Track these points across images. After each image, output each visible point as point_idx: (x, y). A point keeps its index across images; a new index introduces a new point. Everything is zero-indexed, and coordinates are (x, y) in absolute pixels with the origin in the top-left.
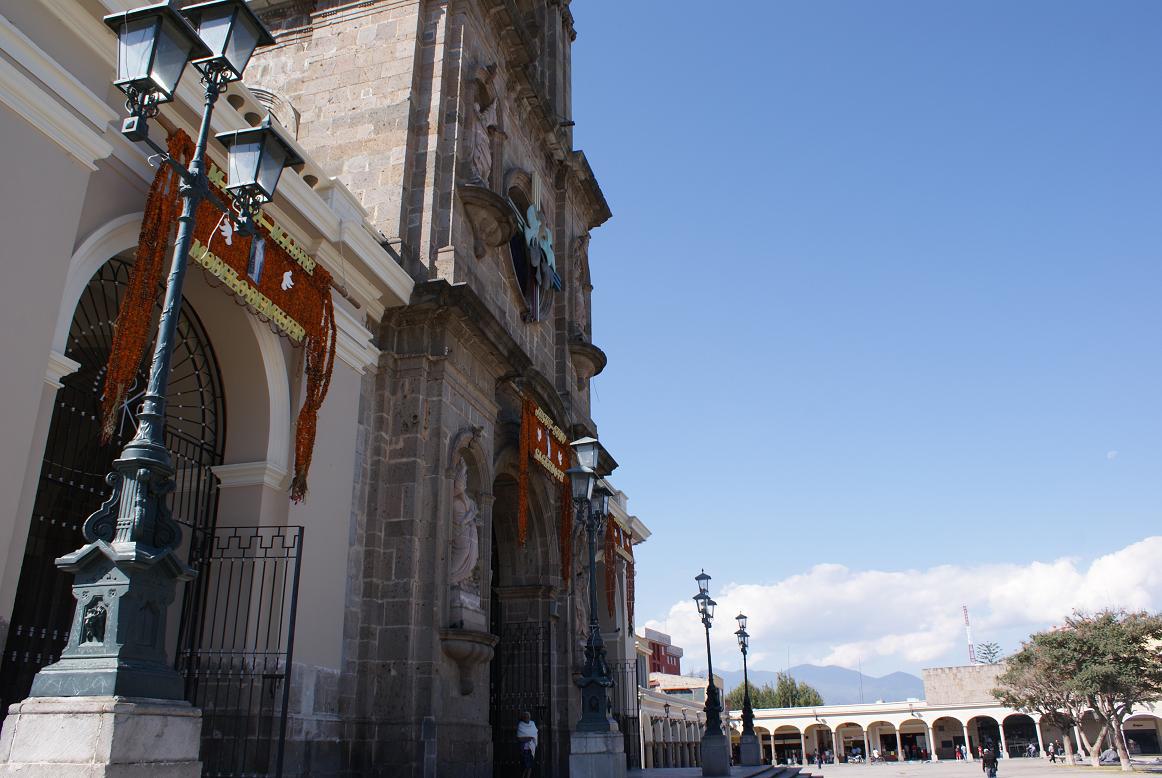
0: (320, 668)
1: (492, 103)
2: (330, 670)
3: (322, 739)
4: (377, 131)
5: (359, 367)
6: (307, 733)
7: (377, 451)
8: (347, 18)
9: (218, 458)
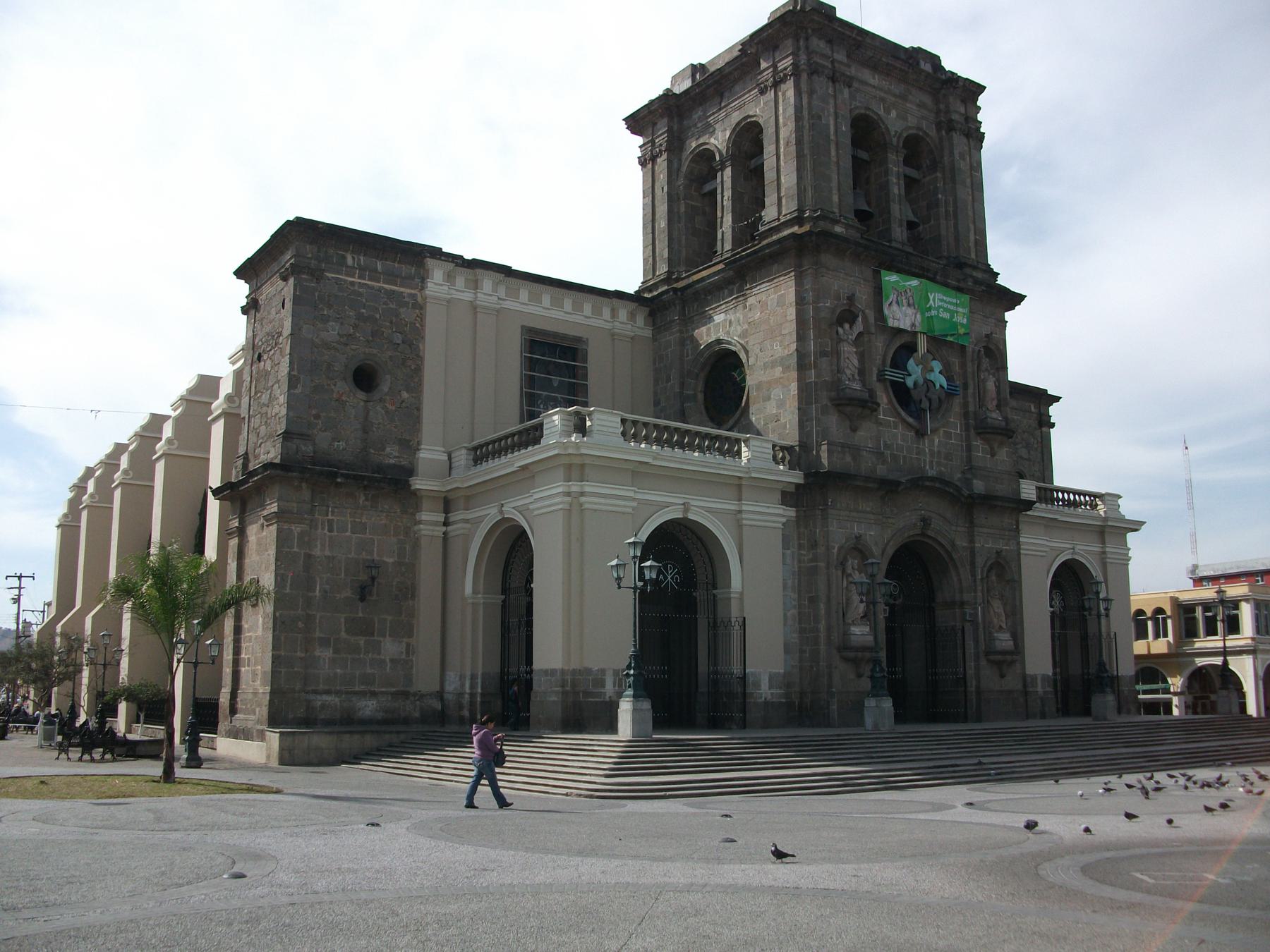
0: (771, 670)
1: (858, 316)
2: (777, 671)
3: (774, 700)
4: (783, 372)
5: (780, 525)
6: (765, 699)
7: (799, 561)
8: (763, 290)
9: (715, 587)
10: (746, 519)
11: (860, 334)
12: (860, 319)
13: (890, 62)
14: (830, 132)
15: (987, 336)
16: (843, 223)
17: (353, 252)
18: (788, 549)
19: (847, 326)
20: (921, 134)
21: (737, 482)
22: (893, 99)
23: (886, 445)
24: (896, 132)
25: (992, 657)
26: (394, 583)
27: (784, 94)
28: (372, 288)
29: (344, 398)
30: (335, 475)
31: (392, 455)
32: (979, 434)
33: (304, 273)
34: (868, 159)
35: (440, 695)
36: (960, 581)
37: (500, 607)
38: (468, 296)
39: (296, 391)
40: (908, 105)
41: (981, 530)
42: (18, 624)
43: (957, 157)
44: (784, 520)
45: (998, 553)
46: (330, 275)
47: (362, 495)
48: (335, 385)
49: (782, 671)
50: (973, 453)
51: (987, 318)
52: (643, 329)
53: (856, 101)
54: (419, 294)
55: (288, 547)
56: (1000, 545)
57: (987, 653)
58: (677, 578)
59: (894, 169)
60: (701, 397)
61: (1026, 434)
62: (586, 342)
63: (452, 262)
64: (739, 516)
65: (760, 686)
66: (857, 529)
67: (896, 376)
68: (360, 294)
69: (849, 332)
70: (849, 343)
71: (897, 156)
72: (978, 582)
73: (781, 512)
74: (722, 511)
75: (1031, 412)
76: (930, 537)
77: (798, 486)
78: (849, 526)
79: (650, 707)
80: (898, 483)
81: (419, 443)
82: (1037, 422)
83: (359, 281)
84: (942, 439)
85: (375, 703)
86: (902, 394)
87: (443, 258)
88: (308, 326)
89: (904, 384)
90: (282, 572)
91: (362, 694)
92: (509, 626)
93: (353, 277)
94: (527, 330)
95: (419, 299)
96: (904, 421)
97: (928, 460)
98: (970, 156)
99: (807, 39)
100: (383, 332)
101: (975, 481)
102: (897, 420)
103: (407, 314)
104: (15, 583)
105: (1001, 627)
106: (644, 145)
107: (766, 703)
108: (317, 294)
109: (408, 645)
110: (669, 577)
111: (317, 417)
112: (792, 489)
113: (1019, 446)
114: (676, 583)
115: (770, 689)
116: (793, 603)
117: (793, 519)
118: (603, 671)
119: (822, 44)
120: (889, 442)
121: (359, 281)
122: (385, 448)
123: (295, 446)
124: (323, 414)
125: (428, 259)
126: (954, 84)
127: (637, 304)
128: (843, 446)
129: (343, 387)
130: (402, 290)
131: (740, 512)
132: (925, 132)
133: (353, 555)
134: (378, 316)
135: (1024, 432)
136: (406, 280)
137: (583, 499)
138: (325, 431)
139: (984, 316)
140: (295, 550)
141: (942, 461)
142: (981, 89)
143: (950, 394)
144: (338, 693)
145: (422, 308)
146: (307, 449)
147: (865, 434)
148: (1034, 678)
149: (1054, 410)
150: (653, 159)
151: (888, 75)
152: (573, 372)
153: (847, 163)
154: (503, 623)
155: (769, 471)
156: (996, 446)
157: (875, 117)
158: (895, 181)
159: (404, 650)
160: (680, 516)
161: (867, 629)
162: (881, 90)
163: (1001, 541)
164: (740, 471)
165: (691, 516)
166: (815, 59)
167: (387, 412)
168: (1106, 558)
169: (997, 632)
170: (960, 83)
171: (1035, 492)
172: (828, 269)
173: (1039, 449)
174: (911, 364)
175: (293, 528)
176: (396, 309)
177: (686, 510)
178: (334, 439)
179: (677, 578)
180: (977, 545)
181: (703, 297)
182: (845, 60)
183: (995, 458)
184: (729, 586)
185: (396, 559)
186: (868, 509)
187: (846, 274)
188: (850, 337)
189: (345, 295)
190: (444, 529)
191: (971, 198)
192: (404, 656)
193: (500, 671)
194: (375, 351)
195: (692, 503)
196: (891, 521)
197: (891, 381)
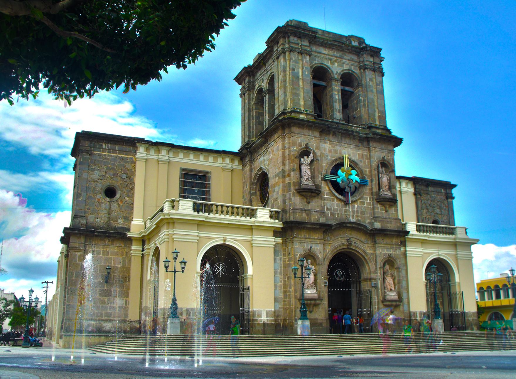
2: (270, 310)
3: (268, 322)
5: (273, 246)
6: (264, 322)
10: (459, 257)
11: (312, 161)
12: (312, 154)
13: (332, 43)
14: (299, 75)
15: (383, 158)
16: (304, 113)
17: (105, 143)
18: (278, 256)
19: (306, 157)
20: (351, 72)
21: (250, 228)
22: (336, 58)
23: (328, 209)
24: (337, 72)
25: (385, 303)
26: (121, 275)
27: (280, 61)
28: (114, 156)
29: (100, 201)
30: (94, 232)
31: (120, 223)
32: (378, 202)
33: (84, 152)
34: (326, 85)
35: (139, 322)
36: (369, 268)
38: (156, 157)
39: (80, 199)
40: (343, 60)
41: (379, 245)
42: (46, 302)
43: (368, 80)
44: (275, 243)
45: (390, 255)
46: (95, 152)
47: (107, 239)
48: (96, 196)
49: (273, 310)
50: (375, 211)
51: (383, 149)
52: (238, 166)
53: (316, 61)
54: (134, 158)
55: (74, 261)
56: (391, 252)
57: (383, 302)
59: (336, 88)
60: (258, 193)
61: (439, 202)
62: (210, 173)
63: (147, 144)
64: (456, 256)
67: (333, 178)
68: (108, 159)
69: (306, 160)
70: (306, 165)
71: (337, 82)
72: (378, 269)
73: (273, 240)
74: (247, 241)
75: (442, 193)
76: (353, 249)
77: (282, 228)
80: (330, 226)
81: (132, 218)
82: (445, 197)
83: (108, 154)
84: (359, 205)
85: (111, 324)
86: (335, 185)
87: (143, 142)
88: (85, 173)
89: (336, 181)
90: (71, 271)
91: (106, 321)
93: (106, 152)
94: (183, 170)
95: (134, 160)
96: (337, 198)
97: (351, 215)
98: (376, 79)
99: (289, 37)
100: (118, 174)
101: (375, 223)
102: (334, 198)
103: (128, 166)
104: (45, 285)
105: (391, 290)
106: (241, 89)
107: (264, 324)
108: (90, 160)
109: (126, 301)
110: (220, 270)
111: (89, 209)
112: (280, 230)
113: (436, 208)
114: (224, 272)
115: (266, 317)
116: (280, 280)
117: (280, 243)
119: (296, 39)
120: (329, 207)
121: (108, 154)
122: (118, 220)
123: (78, 221)
124: (91, 208)
125: (137, 143)
126: (366, 49)
127: (233, 156)
128: (302, 210)
129: (101, 196)
130: (126, 156)
131: (457, 254)
132: (352, 71)
133: (103, 264)
134: (116, 168)
135: (438, 202)
136: (129, 153)
137: (174, 236)
138: (92, 214)
139: (382, 149)
140: (77, 262)
141: (359, 214)
142: (380, 49)
143: (363, 184)
144: (95, 320)
145: (135, 163)
146: (83, 222)
147: (315, 205)
148: (415, 314)
149: (454, 191)
150: (244, 94)
151: (333, 49)
152: (205, 186)
153: (309, 88)
155: (272, 223)
156: (387, 207)
157: (326, 67)
158: (336, 93)
159: (124, 303)
160: (222, 242)
161: (315, 291)
162: (329, 55)
163: (391, 250)
164: (251, 223)
165: (227, 243)
166: (291, 45)
167: (119, 206)
168: (458, 257)
169: (389, 291)
170: (368, 48)
171: (415, 227)
172: (295, 133)
173: (447, 209)
174: (340, 172)
175: (77, 253)
176: (124, 164)
177: (225, 240)
178: (96, 218)
180: (377, 252)
181: (257, 150)
182: (308, 44)
183: (388, 212)
184: (247, 272)
185: (122, 266)
186: (316, 237)
187: (305, 135)
188: (307, 162)
189: (102, 160)
190: (142, 253)
191: (376, 97)
192: (124, 305)
194: (114, 182)
195: (228, 237)
196: (330, 242)
197: (331, 180)
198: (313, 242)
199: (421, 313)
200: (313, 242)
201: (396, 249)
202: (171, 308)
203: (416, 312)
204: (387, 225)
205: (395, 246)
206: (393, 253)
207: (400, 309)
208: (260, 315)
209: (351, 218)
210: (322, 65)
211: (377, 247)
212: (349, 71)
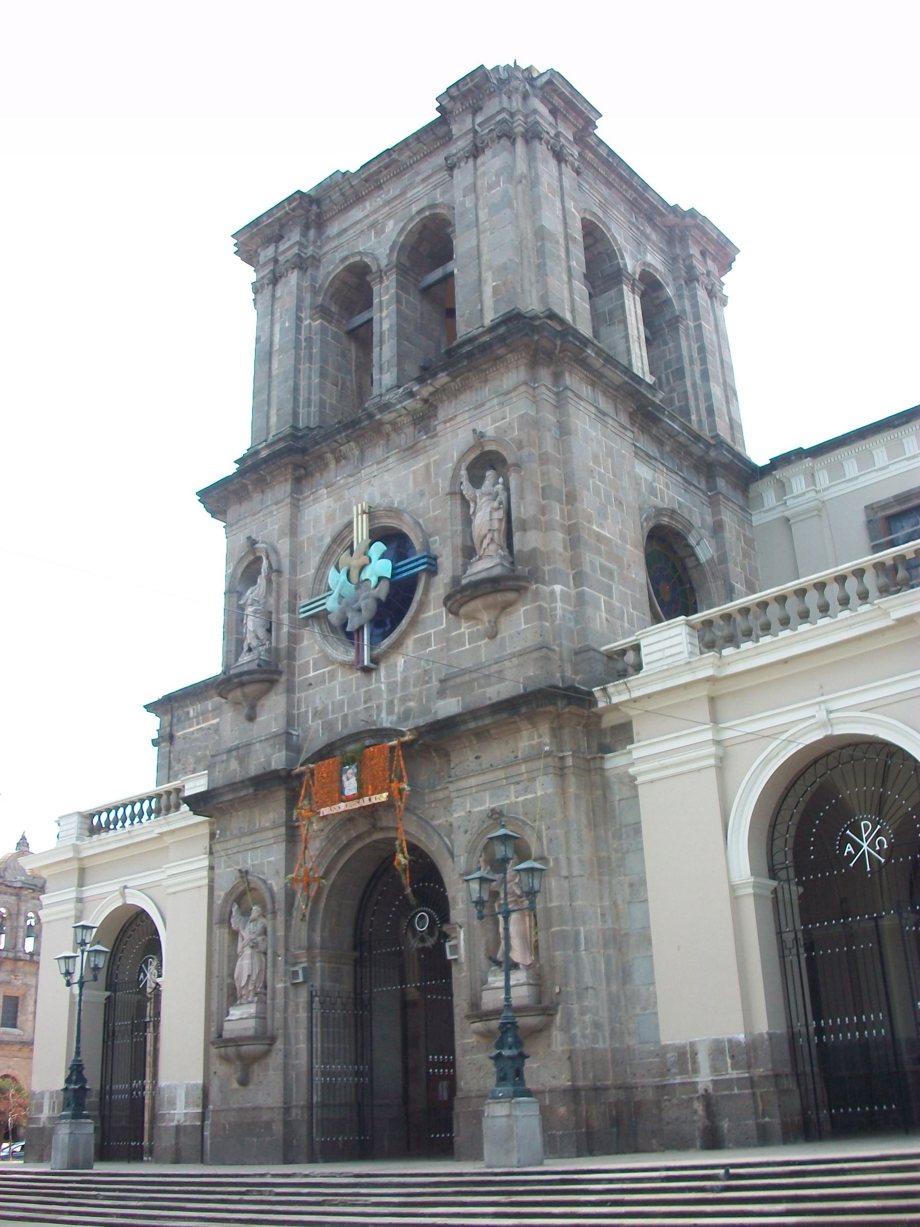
0: (186, 1082)
2: (194, 1082)
6: (178, 1121)
37: (103, 1007)
58: (880, 843)
65: (174, 1104)
66: (252, 860)
78: (240, 861)
79: (538, 1113)
92: (114, 1032)
118: (42, 1094)
154: (106, 1023)
160: (119, 903)
179: (880, 843)
193: (200, 1081)
198: (257, 845)
199: (718, 1050)
200: (257, 845)
201: (533, 779)
202: (66, 1090)
203: (692, 1044)
204: (485, 692)
205: (523, 768)
206: (521, 799)
207: (549, 1046)
208: (172, 1103)
209: (384, 715)
210: (348, 263)
211: (453, 795)
212: (423, 216)
